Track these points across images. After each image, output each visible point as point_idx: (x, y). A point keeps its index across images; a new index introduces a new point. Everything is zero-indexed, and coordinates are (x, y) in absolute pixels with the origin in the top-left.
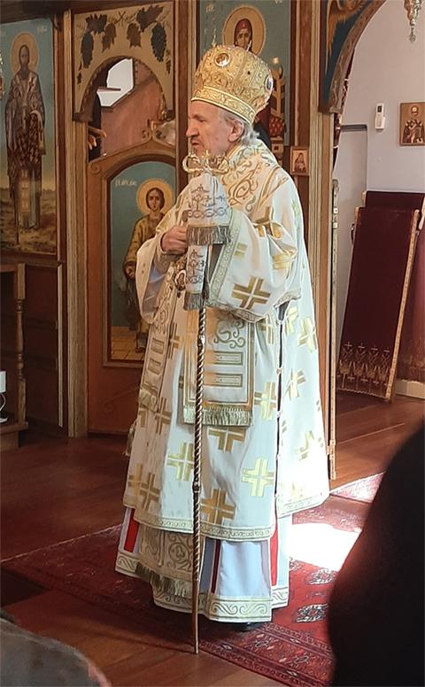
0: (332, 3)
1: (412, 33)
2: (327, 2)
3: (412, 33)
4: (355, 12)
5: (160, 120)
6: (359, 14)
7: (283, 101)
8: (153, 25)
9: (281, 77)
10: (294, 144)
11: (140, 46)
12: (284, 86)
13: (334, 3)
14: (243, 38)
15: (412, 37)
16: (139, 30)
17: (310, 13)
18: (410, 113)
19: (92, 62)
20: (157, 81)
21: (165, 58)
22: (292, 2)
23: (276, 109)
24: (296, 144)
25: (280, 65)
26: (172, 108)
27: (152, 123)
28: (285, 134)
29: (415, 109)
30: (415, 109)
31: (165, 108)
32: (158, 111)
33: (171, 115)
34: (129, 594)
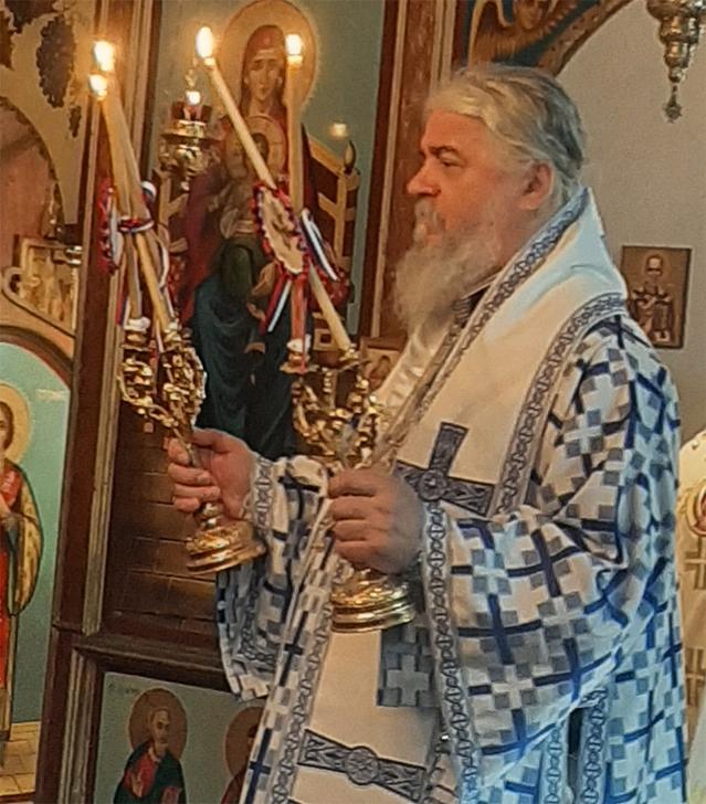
0: (487, 5)
1: (673, 98)
2: (472, 4)
3: (673, 98)
4: (540, 35)
5: (46, 238)
6: (547, 39)
7: (350, 226)
8: (46, 18)
9: (348, 170)
10: (368, 334)
11: (8, 64)
12: (356, 191)
13: (490, 9)
14: (262, 71)
15: (673, 110)
16: (11, 26)
17: (430, 26)
18: (643, 269)
19: (35, 59)
20: (43, 152)
21: (67, 99)
22: (92, 802)
23: (334, 199)
24: (375, 331)
25: (349, 141)
26: (75, 221)
27: (25, 243)
28: (350, 306)
29: (655, 263)
30: (655, 263)
31: (60, 215)
32: (42, 216)
33: (72, 235)
34: (250, 379)
